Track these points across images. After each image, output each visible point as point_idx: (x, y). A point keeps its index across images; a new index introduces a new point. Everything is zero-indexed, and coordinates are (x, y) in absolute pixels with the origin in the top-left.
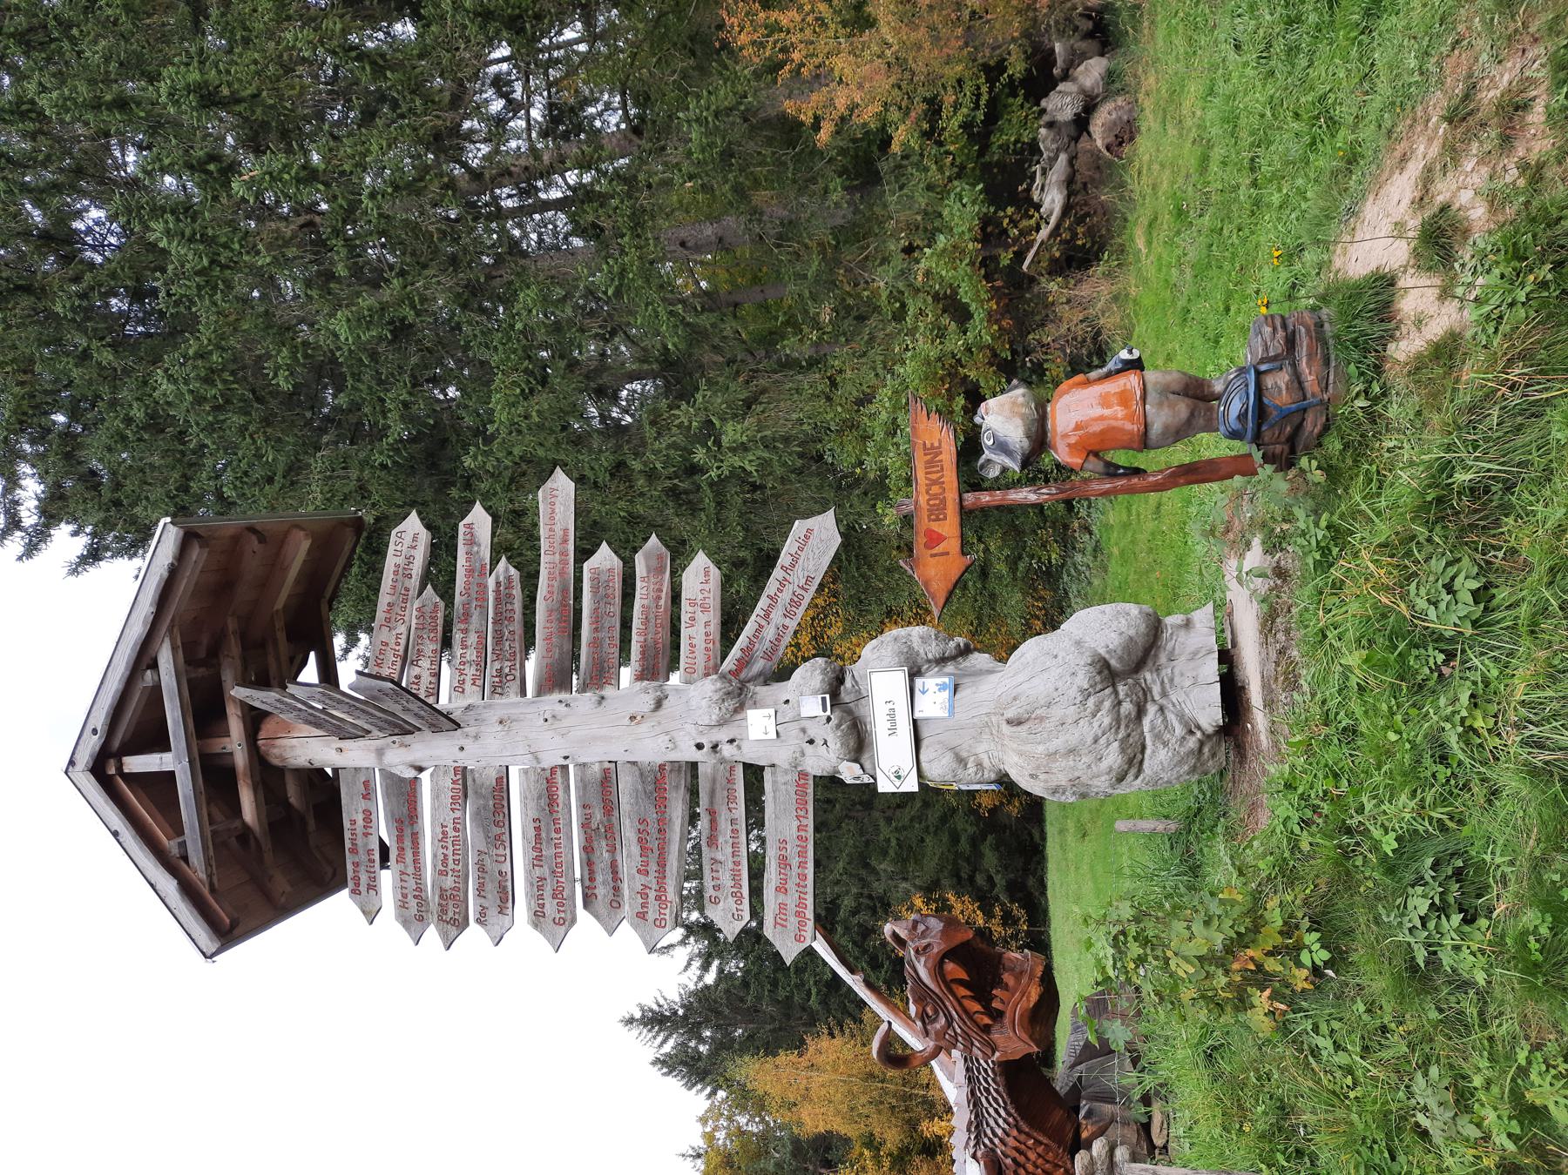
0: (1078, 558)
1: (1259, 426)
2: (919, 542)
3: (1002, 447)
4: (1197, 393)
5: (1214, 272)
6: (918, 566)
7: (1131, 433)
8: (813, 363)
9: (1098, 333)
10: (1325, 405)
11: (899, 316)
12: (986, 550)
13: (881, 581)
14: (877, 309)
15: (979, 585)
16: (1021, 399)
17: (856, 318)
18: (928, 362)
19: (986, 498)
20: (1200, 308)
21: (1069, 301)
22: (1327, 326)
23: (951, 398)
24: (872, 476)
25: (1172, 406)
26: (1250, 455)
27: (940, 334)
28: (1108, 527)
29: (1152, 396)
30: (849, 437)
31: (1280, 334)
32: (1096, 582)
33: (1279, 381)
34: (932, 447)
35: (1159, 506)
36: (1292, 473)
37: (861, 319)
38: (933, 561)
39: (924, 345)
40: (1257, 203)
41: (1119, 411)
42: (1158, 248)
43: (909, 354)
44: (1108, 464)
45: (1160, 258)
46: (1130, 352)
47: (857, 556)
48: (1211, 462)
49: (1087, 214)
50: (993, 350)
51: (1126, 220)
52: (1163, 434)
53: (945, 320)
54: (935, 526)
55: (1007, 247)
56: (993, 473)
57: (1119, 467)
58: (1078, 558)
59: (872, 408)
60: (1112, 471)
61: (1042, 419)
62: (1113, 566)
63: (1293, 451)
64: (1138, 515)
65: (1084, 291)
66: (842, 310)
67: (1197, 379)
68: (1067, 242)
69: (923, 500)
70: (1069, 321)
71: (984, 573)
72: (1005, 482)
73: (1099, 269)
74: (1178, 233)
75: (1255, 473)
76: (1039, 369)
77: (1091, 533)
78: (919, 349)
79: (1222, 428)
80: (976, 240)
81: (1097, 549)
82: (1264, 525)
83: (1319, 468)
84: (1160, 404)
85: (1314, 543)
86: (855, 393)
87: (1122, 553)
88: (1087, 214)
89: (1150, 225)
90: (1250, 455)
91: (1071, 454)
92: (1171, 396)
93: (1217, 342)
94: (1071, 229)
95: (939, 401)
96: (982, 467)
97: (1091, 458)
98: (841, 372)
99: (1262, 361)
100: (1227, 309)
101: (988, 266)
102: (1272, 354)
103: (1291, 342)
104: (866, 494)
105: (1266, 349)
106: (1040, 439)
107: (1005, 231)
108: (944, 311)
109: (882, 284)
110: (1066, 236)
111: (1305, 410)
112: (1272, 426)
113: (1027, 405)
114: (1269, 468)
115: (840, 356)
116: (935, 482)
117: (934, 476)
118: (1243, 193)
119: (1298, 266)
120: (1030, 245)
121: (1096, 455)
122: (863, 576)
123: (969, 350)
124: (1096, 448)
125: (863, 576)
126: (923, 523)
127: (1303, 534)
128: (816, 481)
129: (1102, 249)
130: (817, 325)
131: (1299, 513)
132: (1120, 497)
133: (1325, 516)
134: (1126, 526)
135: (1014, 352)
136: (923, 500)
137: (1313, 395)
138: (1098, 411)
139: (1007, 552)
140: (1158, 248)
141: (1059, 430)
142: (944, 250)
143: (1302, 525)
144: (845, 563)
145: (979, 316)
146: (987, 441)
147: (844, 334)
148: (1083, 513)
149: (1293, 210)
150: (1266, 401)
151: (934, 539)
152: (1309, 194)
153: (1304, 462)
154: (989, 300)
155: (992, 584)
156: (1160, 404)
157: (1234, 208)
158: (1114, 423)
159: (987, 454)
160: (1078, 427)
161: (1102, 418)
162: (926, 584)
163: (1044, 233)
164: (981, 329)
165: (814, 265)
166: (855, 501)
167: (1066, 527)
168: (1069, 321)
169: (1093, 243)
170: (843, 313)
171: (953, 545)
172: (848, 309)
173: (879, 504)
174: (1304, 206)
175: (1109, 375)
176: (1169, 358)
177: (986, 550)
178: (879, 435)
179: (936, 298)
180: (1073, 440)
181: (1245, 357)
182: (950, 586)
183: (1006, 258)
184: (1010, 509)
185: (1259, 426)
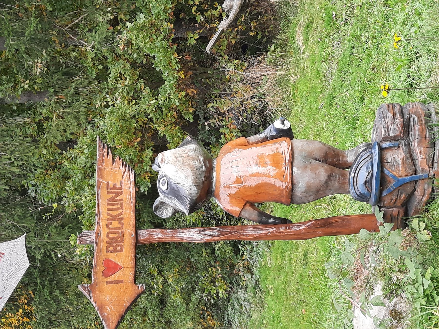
0: (241, 293)
1: (381, 192)
2: (98, 269)
3: (174, 192)
4: (334, 161)
5: (354, 69)
6: (94, 291)
7: (280, 189)
8: (22, 109)
9: (265, 107)
10: (431, 178)
11: (102, 76)
12: (165, 282)
13: (71, 304)
14: (83, 69)
15: (157, 313)
16: (192, 153)
17: (65, 74)
18: (124, 118)
19: (158, 235)
20: (342, 96)
21: (242, 80)
22: (434, 117)
23: (142, 150)
24: (69, 211)
25: (314, 170)
26: (373, 215)
27: (136, 97)
28: (266, 269)
29: (298, 160)
30: (53, 175)
31: (399, 119)
32: (255, 315)
33: (396, 156)
34: (115, 187)
35: (306, 253)
36: (406, 232)
37: (69, 75)
38: (108, 287)
39: (120, 102)
40: (387, 19)
41: (271, 170)
42: (313, 46)
43: (109, 109)
44: (262, 214)
45: (314, 54)
46: (283, 123)
47: (51, 281)
48: (343, 218)
49: (260, 13)
50: (179, 112)
51: (289, 21)
52: (306, 192)
53: (141, 84)
54: (113, 257)
55: (194, 30)
56: (166, 214)
57: (270, 217)
58: (241, 293)
59: (72, 153)
60: (264, 220)
61: (209, 171)
62: (269, 302)
63: (406, 214)
64: (290, 260)
65: (255, 73)
66: (52, 66)
67: (334, 150)
68: (244, 33)
69: (103, 233)
70: (242, 95)
71: (162, 302)
72: (177, 220)
73: (267, 58)
74: (329, 35)
75: (376, 230)
76: (216, 133)
77: (252, 274)
78: (118, 105)
79: (352, 191)
80: (169, 21)
81: (257, 287)
82: (384, 274)
83: (426, 229)
84: (305, 168)
85: (421, 291)
86: (59, 138)
87: (276, 292)
88: (260, 13)
89: (307, 27)
90: (373, 215)
91: (231, 202)
92: (313, 162)
93: (354, 124)
94: (247, 24)
95: (131, 151)
96: (157, 208)
97: (248, 207)
98: (47, 119)
99: (385, 139)
100: (363, 98)
101: (179, 43)
102: (392, 135)
103: (406, 126)
104: (63, 226)
105: (388, 131)
106: (206, 188)
107: (194, 19)
108: (140, 77)
109: (89, 48)
110: (242, 28)
111: (416, 182)
112: (391, 192)
113: (197, 159)
114: (388, 226)
115: (47, 105)
116: (115, 218)
117: (115, 213)
118: (377, 10)
119: (414, 70)
120: (212, 31)
121: (252, 205)
122: (55, 299)
123: (159, 109)
124: (253, 199)
125: (55, 299)
126: (103, 253)
127: (413, 283)
128: (19, 211)
129: (270, 42)
130: (28, 75)
131: (410, 265)
132: (277, 243)
133: (430, 269)
134: (280, 268)
135: (196, 117)
136: (103, 233)
137: (422, 170)
138: (256, 169)
139: (182, 285)
140: (313, 46)
141: (223, 182)
142: (143, 26)
143: (412, 275)
144: (39, 287)
145: (168, 84)
146: (162, 186)
147: (53, 86)
148: (246, 256)
149: (412, 26)
150: (386, 172)
151: (111, 268)
152: (424, 15)
153: (415, 223)
154: (179, 71)
155: (169, 312)
156: (305, 168)
157: (371, 20)
158: (267, 180)
159: (162, 197)
160: (238, 181)
161: (257, 175)
162: (101, 308)
163: (224, 24)
164: (171, 93)
165: (32, 26)
166: (53, 231)
167: (232, 266)
168: (242, 95)
169: (263, 37)
170: (53, 69)
171: (127, 273)
172: (59, 64)
173: (73, 237)
174: (420, 23)
175: (265, 140)
176: (318, 133)
177: (165, 282)
178: (77, 177)
179: (134, 65)
180: (233, 191)
181: (373, 137)
182: (122, 311)
183: (192, 38)
184: (183, 246)
185: (381, 192)
